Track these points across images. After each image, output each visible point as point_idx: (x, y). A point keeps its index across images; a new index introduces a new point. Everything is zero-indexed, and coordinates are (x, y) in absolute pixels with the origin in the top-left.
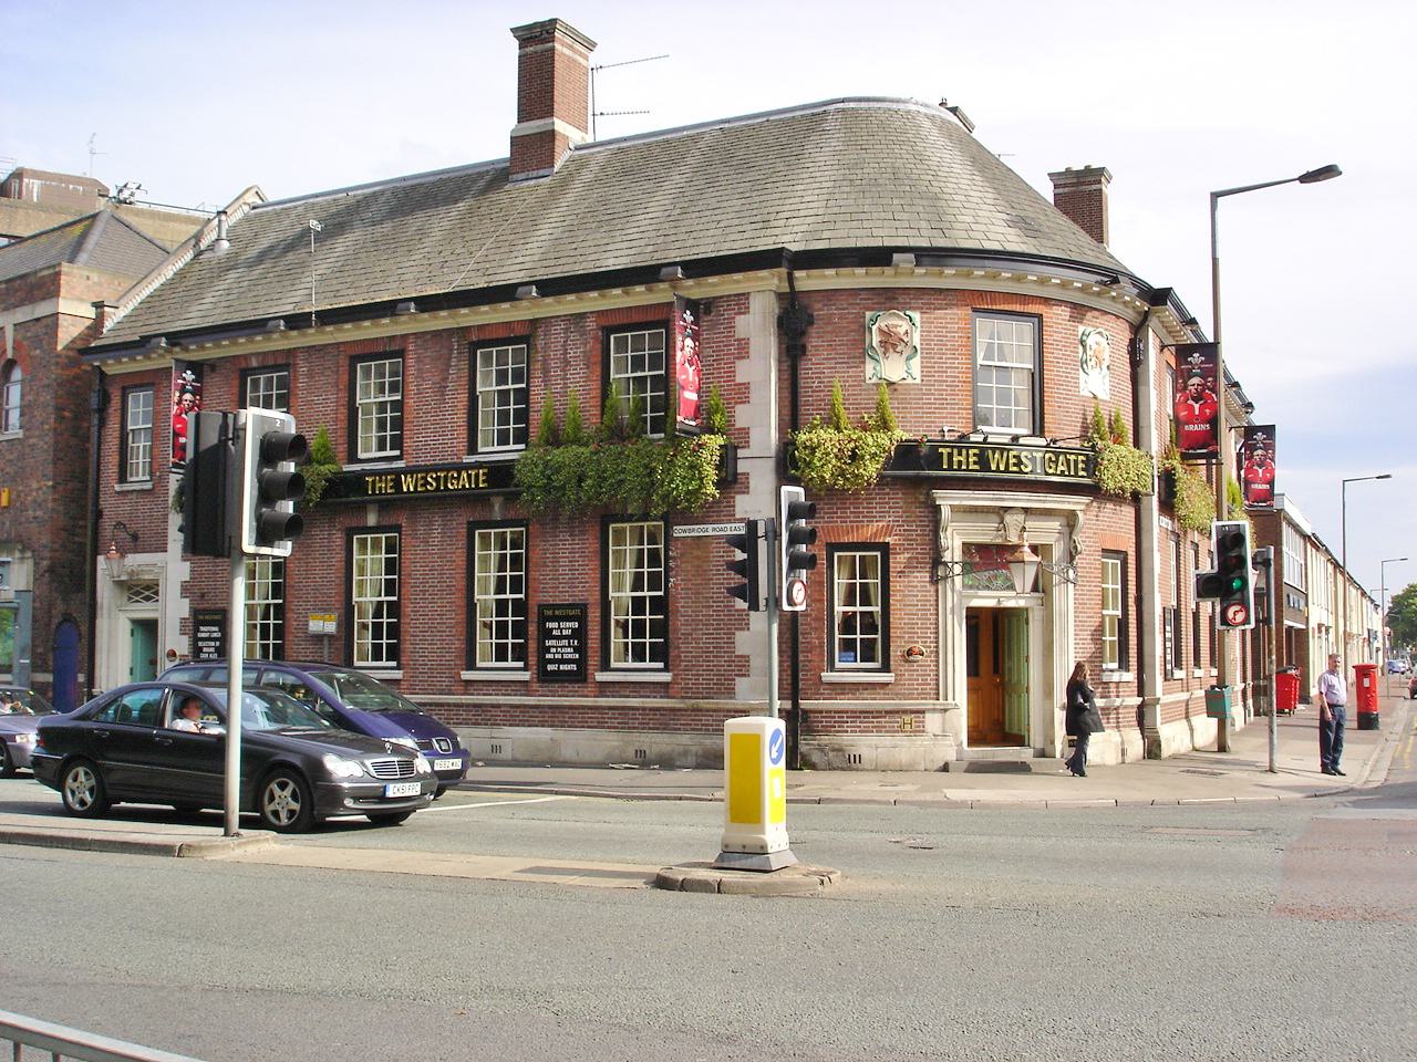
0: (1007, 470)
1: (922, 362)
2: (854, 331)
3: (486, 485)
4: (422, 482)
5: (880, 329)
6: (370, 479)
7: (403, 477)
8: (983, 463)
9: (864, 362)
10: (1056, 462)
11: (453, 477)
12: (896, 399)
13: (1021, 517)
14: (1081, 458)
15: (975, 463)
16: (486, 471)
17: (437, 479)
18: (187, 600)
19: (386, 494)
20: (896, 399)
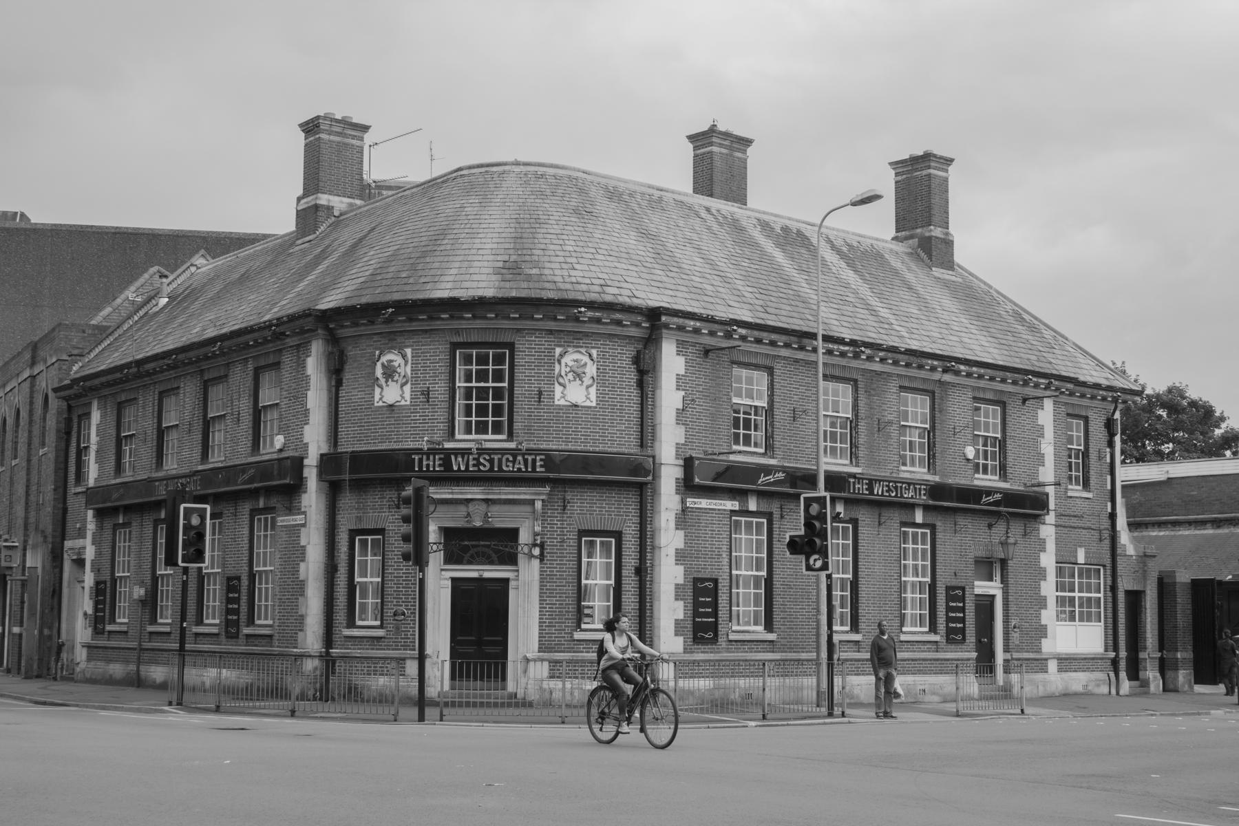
0: (882, 495)
1: (412, 388)
2: (368, 366)
3: (442, 469)
4: (475, 462)
5: (383, 365)
6: (852, 480)
7: (453, 457)
8: (447, 464)
9: (374, 390)
10: (909, 489)
11: (507, 460)
12: (394, 417)
13: (483, 507)
14: (922, 487)
15: (541, 466)
16: (442, 456)
17: (491, 461)
18: (682, 568)
19: (863, 494)
20: (394, 417)
